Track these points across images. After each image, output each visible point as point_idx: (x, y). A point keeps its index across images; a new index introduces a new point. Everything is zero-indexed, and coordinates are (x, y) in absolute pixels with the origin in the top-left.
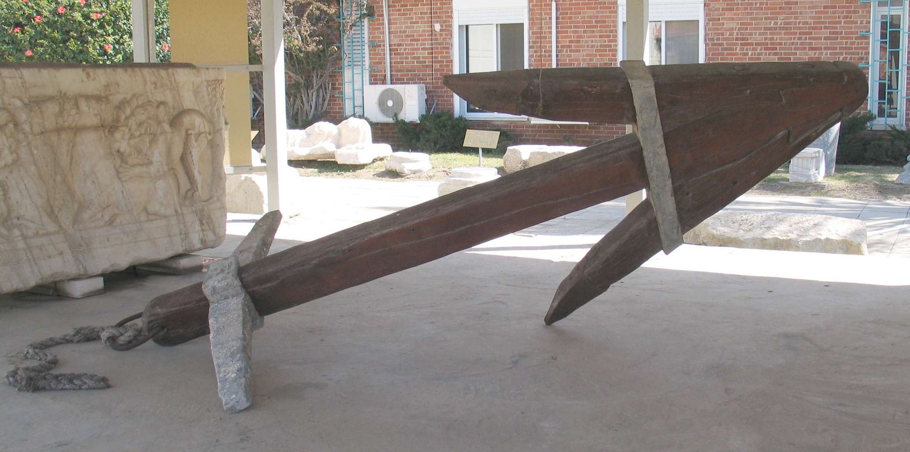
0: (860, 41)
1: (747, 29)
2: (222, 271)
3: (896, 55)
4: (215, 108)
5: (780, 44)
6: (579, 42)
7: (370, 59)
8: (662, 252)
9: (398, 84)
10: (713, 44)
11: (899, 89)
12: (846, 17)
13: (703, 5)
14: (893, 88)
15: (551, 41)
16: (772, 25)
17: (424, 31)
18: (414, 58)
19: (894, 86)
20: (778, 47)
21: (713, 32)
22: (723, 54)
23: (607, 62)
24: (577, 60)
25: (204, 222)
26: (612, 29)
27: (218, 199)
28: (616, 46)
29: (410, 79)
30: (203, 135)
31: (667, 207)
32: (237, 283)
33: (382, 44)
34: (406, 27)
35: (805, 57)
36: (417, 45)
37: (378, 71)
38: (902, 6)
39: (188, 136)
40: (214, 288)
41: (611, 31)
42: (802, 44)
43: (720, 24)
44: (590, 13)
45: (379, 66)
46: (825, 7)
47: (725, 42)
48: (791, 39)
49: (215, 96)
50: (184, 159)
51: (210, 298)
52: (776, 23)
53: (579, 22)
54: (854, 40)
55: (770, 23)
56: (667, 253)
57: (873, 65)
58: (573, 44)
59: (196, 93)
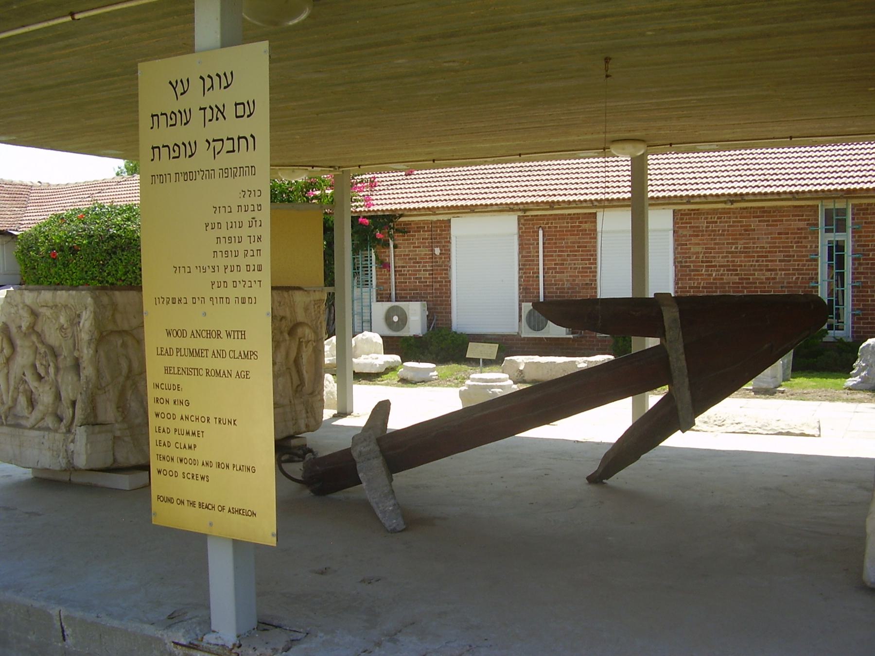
0: (810, 263)
1: (711, 253)
2: (365, 440)
3: (841, 276)
4: (319, 322)
5: (741, 266)
6: (563, 264)
7: (377, 279)
8: (679, 432)
9: (402, 301)
10: (681, 266)
11: (845, 305)
12: (798, 242)
13: (672, 232)
14: (840, 304)
15: (539, 264)
16: (733, 249)
17: (425, 254)
18: (416, 278)
19: (841, 303)
20: (739, 268)
21: (682, 256)
22: (690, 275)
23: (588, 282)
24: (561, 280)
25: (309, 410)
26: (592, 253)
27: (319, 393)
28: (596, 268)
29: (413, 297)
30: (310, 343)
31: (685, 397)
32: (377, 448)
33: (855, 302)
34: (409, 251)
35: (762, 277)
36: (419, 266)
37: (384, 290)
38: (845, 232)
39: (300, 343)
40: (360, 452)
41: (592, 255)
42: (759, 265)
43: (687, 249)
44: (572, 239)
45: (385, 285)
46: (779, 234)
47: (692, 264)
48: (749, 261)
49: (319, 312)
50: (297, 362)
51: (357, 459)
52: (736, 248)
53: (563, 247)
54: (805, 263)
55: (731, 248)
56: (683, 432)
57: (821, 284)
58: (558, 267)
59: (306, 309)
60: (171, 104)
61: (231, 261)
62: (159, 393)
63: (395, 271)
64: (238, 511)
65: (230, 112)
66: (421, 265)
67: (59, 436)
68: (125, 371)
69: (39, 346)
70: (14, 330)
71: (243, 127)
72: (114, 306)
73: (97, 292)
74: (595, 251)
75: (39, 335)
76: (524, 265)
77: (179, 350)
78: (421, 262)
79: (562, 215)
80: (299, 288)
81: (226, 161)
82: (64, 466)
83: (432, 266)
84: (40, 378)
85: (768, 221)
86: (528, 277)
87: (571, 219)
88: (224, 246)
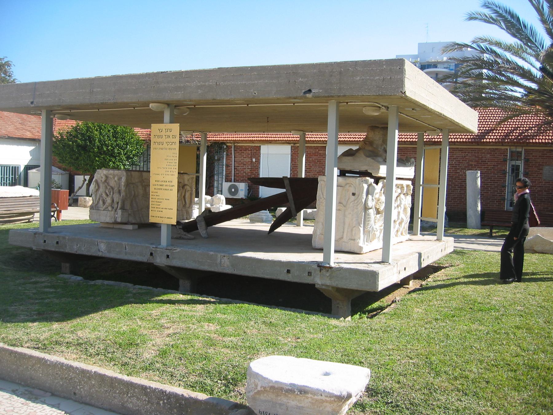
6: (310, 169)
7: (226, 171)
17: (248, 161)
28: (325, 171)
34: (241, 159)
41: (323, 165)
50: (184, 197)
53: (310, 161)
57: (508, 186)
59: (188, 180)
60: (159, 134)
61: (170, 167)
62: (153, 194)
63: (234, 168)
64: (169, 218)
65: (171, 137)
66: (246, 166)
67: (113, 212)
68: (133, 195)
69: (108, 186)
70: (99, 181)
71: (174, 140)
72: (131, 175)
73: (127, 172)
74: (325, 163)
75: (108, 183)
76: (293, 168)
77: (158, 185)
78: (246, 165)
79: (311, 146)
80: (186, 173)
81: (169, 146)
82: (113, 221)
83: (251, 167)
84: (107, 195)
85: (401, 153)
86: (295, 174)
87: (315, 148)
88: (169, 164)
